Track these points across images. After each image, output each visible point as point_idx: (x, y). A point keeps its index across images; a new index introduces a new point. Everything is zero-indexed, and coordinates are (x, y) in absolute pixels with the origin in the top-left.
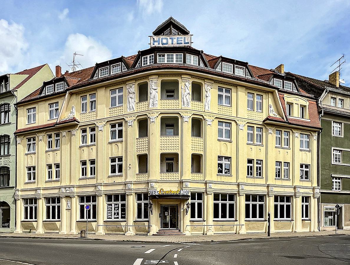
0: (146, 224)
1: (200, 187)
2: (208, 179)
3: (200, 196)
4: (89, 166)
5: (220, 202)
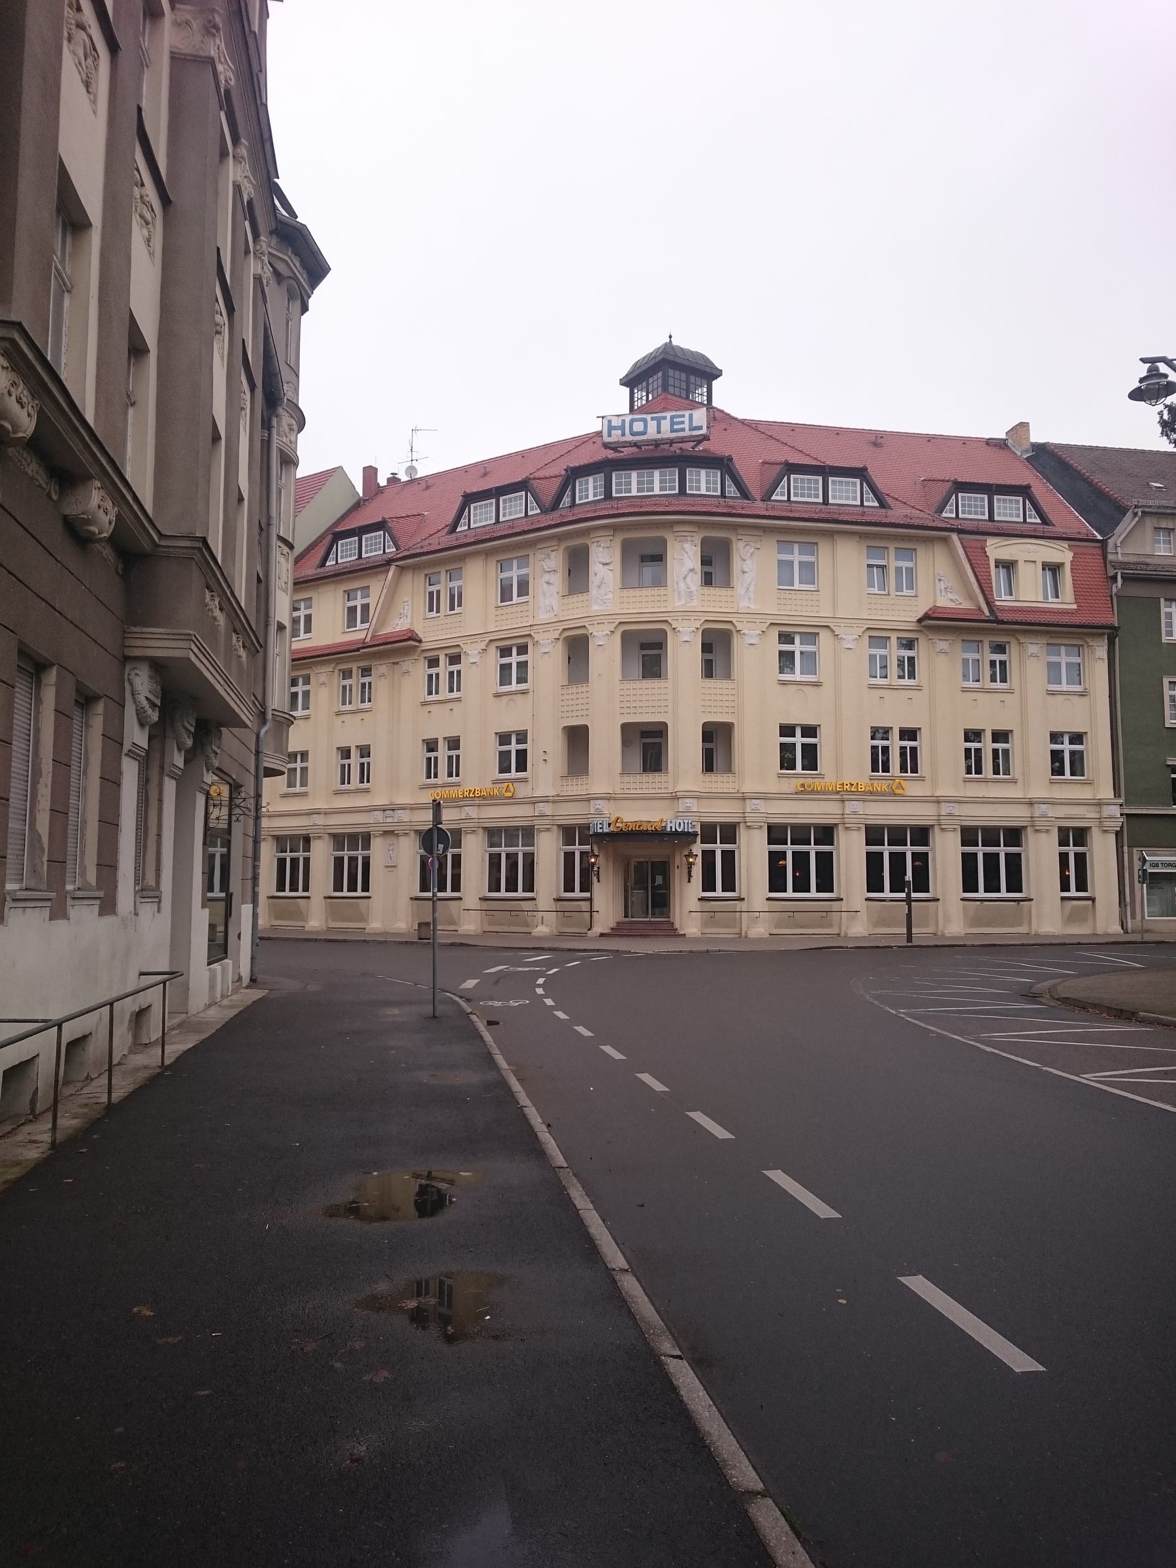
0: (585, 906)
1: (721, 812)
2: (748, 787)
3: (729, 832)
4: (442, 753)
5: (789, 849)
